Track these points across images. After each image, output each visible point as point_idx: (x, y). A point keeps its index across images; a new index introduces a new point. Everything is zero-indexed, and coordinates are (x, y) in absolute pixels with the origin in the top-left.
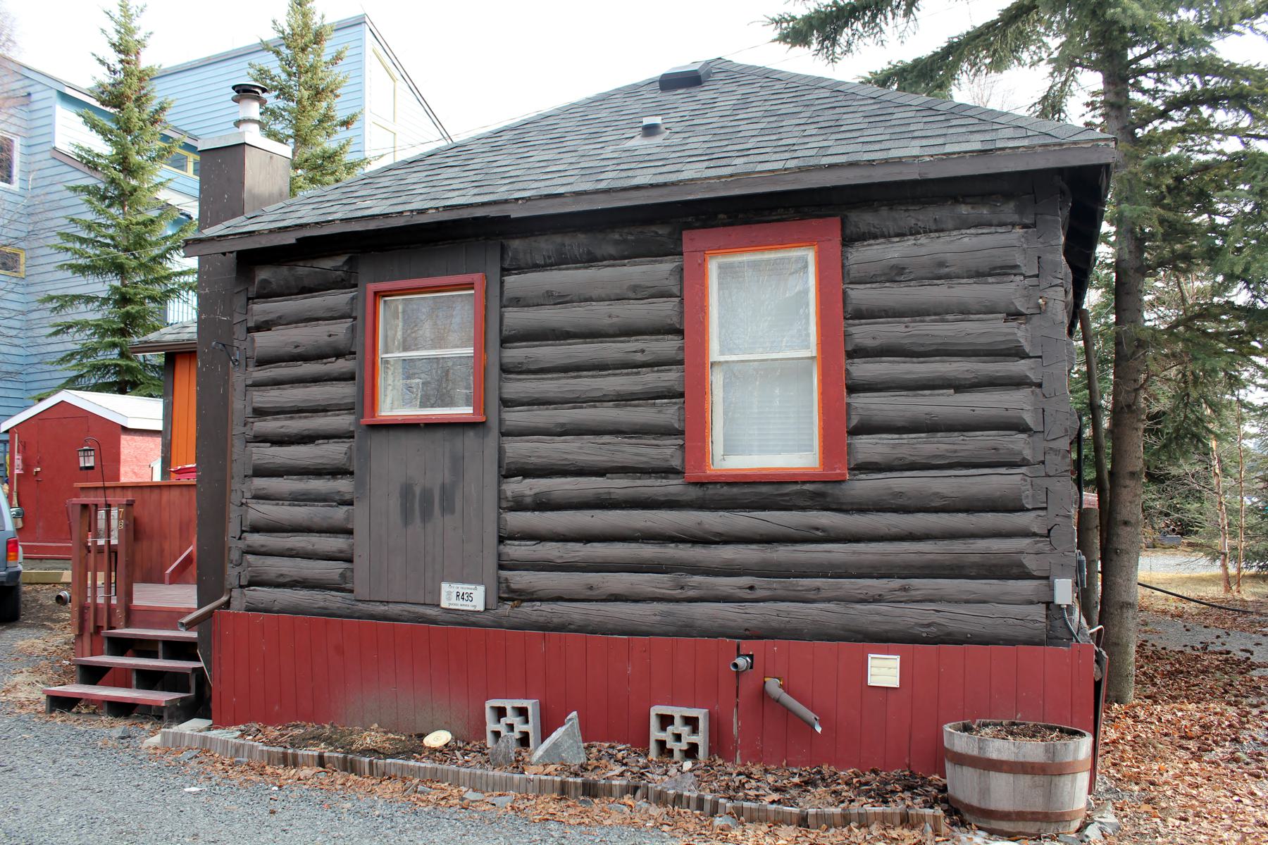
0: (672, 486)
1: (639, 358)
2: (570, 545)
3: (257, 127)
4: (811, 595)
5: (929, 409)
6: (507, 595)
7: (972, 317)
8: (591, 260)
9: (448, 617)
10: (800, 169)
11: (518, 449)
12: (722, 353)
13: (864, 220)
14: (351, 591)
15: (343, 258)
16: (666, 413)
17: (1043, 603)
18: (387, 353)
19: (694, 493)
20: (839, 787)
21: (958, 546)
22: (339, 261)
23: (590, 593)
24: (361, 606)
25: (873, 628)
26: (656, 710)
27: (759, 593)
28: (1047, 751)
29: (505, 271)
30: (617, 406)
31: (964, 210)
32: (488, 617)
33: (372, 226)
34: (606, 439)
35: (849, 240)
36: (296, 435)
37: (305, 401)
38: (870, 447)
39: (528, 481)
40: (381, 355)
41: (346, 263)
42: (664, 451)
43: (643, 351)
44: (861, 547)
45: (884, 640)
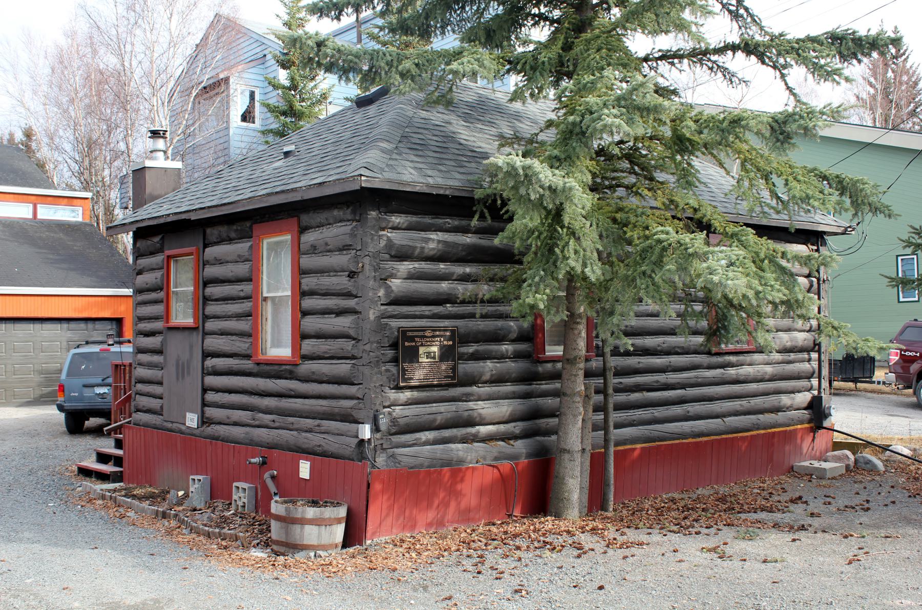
0: (247, 364)
1: (242, 294)
2: (324, 385)
3: (162, 153)
4: (291, 426)
5: (320, 326)
6: (205, 421)
7: (339, 273)
8: (230, 240)
9: (188, 431)
10: (269, 195)
11: (213, 343)
12: (268, 291)
13: (305, 219)
14: (162, 415)
15: (160, 237)
16: (243, 325)
17: (825, 428)
18: (176, 288)
19: (256, 369)
20: (410, 540)
21: (333, 403)
22: (157, 239)
23: (228, 420)
24: (165, 424)
25: (304, 446)
26: (235, 484)
27: (277, 424)
28: (286, 510)
29: (206, 246)
30: (237, 320)
31: (336, 213)
32: (197, 432)
33: (162, 221)
34: (234, 338)
35: (303, 230)
36: (149, 331)
37: (151, 313)
38: (308, 346)
39: (214, 359)
40: (173, 289)
41: (161, 239)
42: (241, 345)
43: (242, 291)
44: (307, 401)
45: (307, 452)
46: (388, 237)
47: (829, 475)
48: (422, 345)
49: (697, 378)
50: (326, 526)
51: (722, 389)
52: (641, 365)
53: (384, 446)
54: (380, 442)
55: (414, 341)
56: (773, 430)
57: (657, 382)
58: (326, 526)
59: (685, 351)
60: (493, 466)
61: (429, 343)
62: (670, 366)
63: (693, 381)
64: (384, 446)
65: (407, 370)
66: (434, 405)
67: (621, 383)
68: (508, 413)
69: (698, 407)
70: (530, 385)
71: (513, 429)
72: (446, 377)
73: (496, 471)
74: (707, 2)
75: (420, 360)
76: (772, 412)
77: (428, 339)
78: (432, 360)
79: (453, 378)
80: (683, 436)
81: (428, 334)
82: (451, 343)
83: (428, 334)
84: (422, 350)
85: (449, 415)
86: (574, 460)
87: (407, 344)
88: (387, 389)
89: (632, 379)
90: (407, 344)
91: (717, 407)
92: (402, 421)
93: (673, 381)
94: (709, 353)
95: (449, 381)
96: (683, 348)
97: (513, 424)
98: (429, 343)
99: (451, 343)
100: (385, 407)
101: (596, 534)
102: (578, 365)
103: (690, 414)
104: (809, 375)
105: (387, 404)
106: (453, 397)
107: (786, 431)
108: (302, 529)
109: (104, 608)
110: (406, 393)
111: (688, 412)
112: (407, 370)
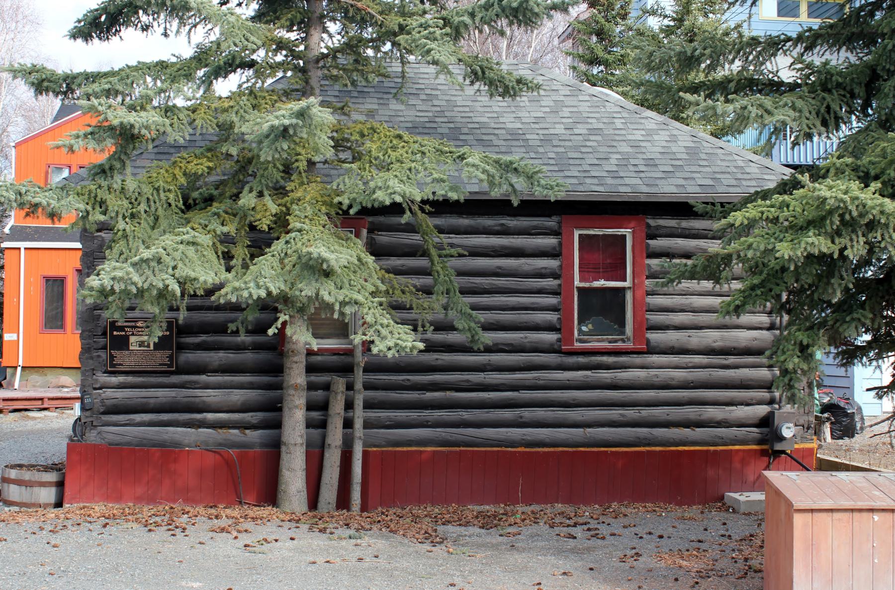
46: (103, 238)
47: (743, 509)
48: (133, 334)
49: (539, 379)
50: (26, 487)
51: (685, 394)
52: (439, 362)
53: (94, 424)
54: (91, 419)
55: (124, 331)
56: (680, 448)
57: (468, 381)
58: (26, 487)
59: (536, 349)
60: (215, 452)
61: (141, 333)
62: (489, 365)
63: (527, 383)
64: (94, 424)
65: (116, 357)
66: (153, 390)
67: (408, 380)
68: (239, 403)
69: (543, 412)
70: (277, 376)
71: (249, 419)
72: (160, 365)
73: (217, 456)
74: (339, 2)
75: (131, 348)
76: (688, 427)
77: (140, 330)
78: (146, 349)
79: (170, 366)
80: (513, 444)
81: (139, 324)
82: (168, 333)
83: (139, 324)
84: (133, 339)
85: (164, 400)
86: (290, 453)
87: (115, 333)
88: (99, 374)
89: (427, 377)
90: (115, 333)
91: (527, 414)
92: (108, 402)
93: (495, 382)
94: (559, 351)
95: (165, 368)
96: (511, 345)
97: (250, 414)
98: (141, 333)
99: (168, 333)
100: (95, 389)
101: (459, 544)
102: (291, 358)
103: (523, 420)
104: (769, 385)
105: (98, 386)
106: (174, 383)
107: (707, 451)
108: (8, 487)
109: (321, 587)
110: (119, 378)
111: (521, 417)
112: (116, 357)
